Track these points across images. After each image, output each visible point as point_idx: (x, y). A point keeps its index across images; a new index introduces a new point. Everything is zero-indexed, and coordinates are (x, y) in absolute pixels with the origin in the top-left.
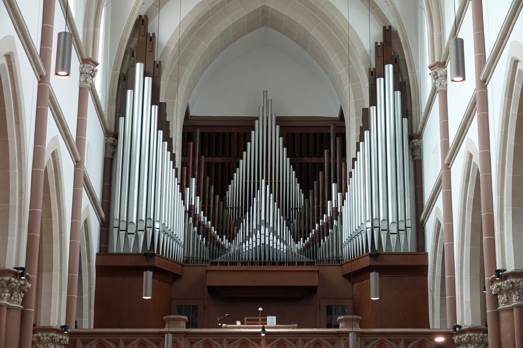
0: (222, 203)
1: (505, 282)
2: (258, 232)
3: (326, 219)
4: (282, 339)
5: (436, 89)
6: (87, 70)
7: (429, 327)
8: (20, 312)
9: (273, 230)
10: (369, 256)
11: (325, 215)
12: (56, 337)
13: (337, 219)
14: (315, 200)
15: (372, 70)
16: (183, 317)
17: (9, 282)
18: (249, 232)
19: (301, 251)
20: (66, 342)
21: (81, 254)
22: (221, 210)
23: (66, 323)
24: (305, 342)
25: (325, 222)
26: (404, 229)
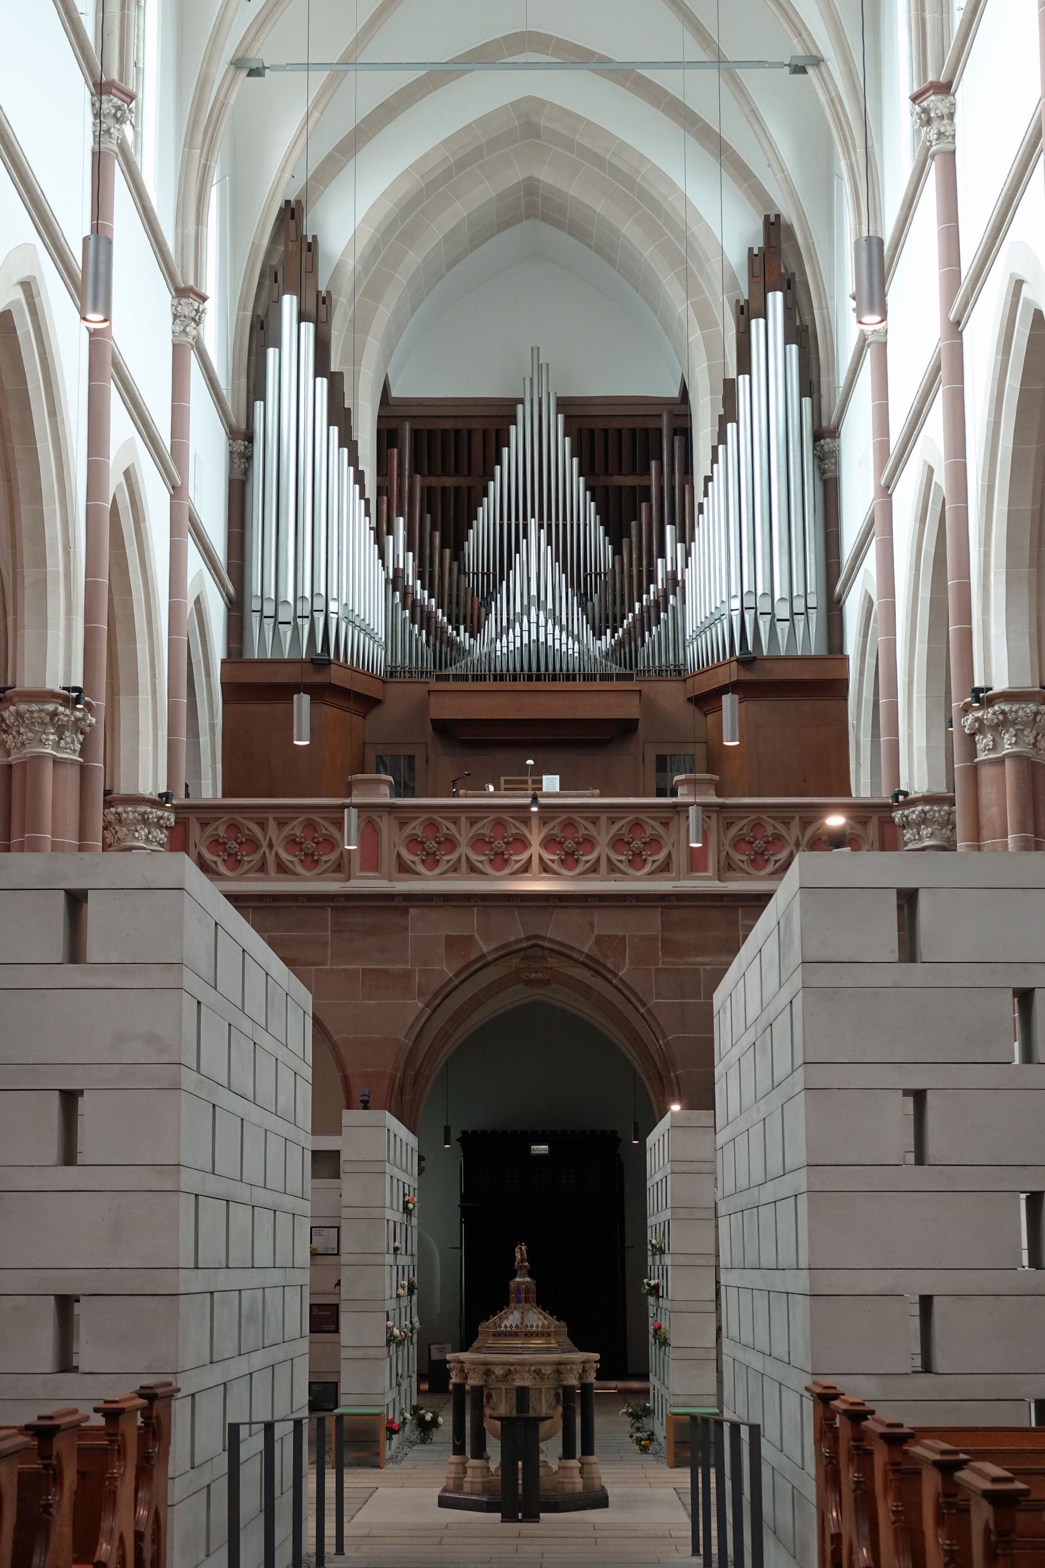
0: (456, 564)
1: (990, 710)
2: (525, 618)
3: (654, 592)
4: (570, 817)
5: (865, 340)
6: (186, 310)
7: (849, 795)
8: (78, 768)
9: (554, 614)
10: (735, 663)
11: (652, 586)
12: (151, 813)
13: (675, 594)
14: (634, 556)
15: (742, 303)
16: (384, 777)
17: (55, 714)
18: (508, 619)
19: (607, 654)
20: (171, 823)
21: (193, 661)
22: (455, 577)
23: (168, 789)
24: (613, 823)
25: (652, 598)
26: (803, 610)
